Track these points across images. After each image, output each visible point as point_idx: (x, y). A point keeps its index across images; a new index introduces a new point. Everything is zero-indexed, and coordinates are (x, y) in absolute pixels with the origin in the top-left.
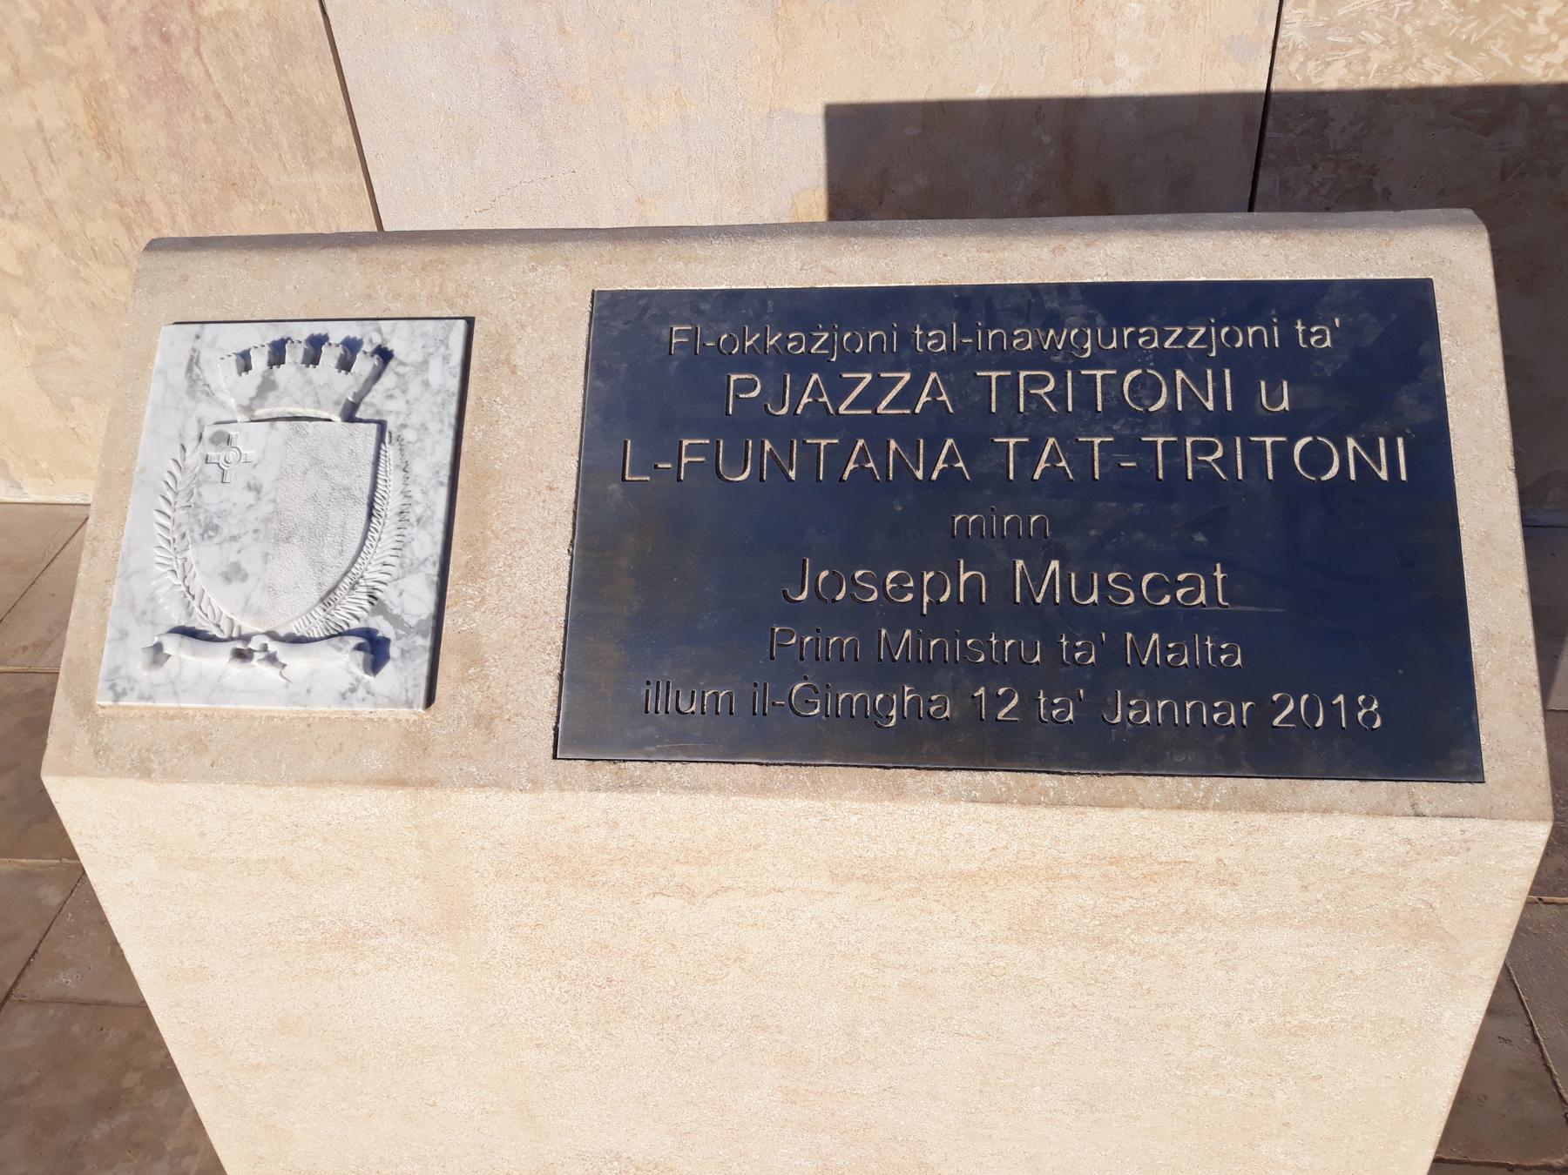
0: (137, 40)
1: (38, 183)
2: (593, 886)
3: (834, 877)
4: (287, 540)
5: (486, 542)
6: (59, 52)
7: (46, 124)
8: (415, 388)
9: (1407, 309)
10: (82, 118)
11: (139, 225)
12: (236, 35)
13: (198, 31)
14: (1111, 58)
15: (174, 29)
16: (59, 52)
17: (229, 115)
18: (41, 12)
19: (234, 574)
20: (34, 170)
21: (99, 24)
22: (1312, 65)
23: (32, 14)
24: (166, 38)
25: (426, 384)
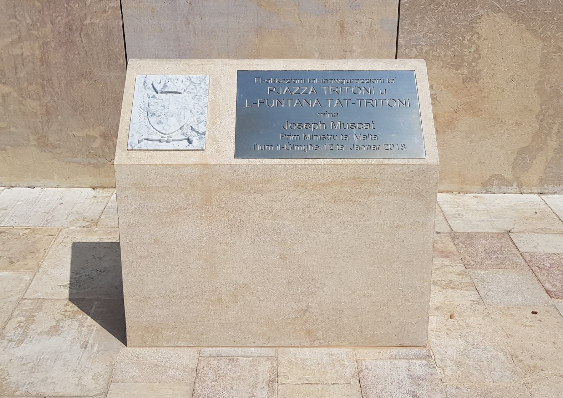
0: (61, 30)
1: (16, 72)
2: (240, 191)
3: (295, 186)
4: (172, 116)
5: (216, 118)
6: (35, 33)
7: (24, 54)
8: (198, 88)
9: (410, 75)
10: (37, 52)
11: (47, 87)
12: (93, 29)
13: (82, 28)
14: (352, 47)
15: (74, 27)
16: (35, 33)
17: (86, 53)
18: (32, 21)
19: (160, 123)
20: (16, 68)
21: (51, 25)
22: (407, 50)
23: (29, 21)
24: (71, 30)
25: (201, 87)
